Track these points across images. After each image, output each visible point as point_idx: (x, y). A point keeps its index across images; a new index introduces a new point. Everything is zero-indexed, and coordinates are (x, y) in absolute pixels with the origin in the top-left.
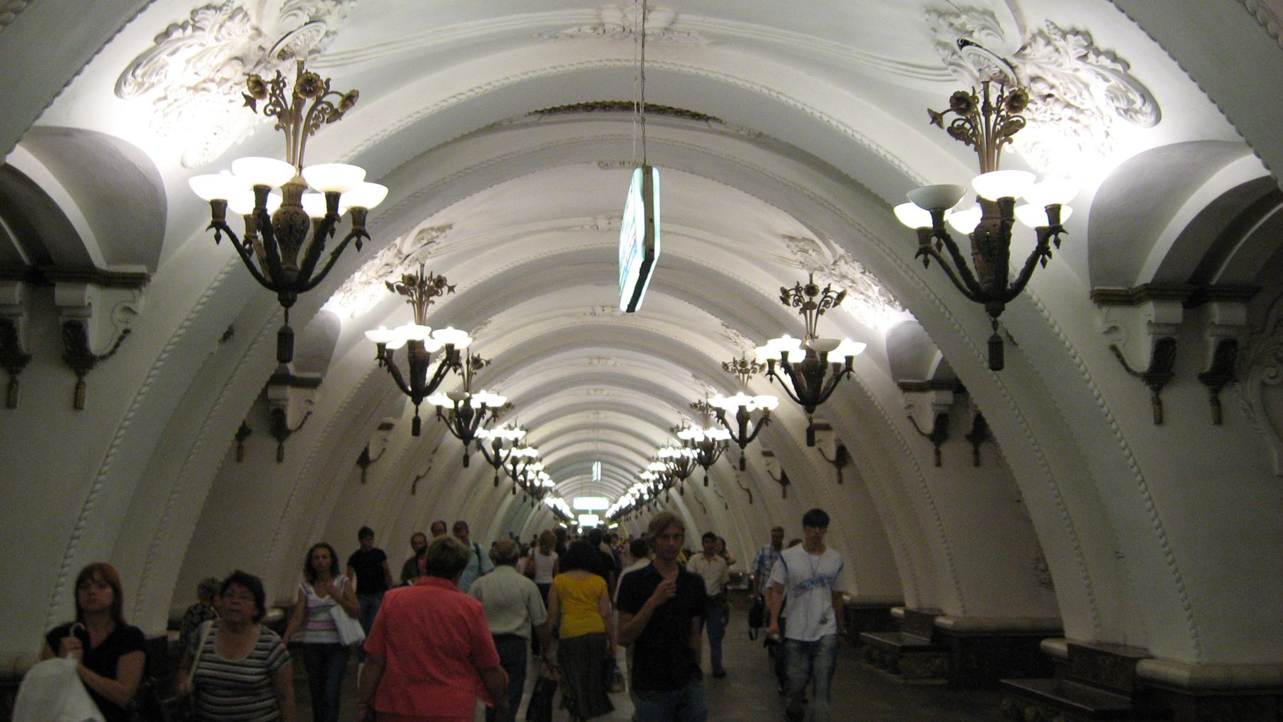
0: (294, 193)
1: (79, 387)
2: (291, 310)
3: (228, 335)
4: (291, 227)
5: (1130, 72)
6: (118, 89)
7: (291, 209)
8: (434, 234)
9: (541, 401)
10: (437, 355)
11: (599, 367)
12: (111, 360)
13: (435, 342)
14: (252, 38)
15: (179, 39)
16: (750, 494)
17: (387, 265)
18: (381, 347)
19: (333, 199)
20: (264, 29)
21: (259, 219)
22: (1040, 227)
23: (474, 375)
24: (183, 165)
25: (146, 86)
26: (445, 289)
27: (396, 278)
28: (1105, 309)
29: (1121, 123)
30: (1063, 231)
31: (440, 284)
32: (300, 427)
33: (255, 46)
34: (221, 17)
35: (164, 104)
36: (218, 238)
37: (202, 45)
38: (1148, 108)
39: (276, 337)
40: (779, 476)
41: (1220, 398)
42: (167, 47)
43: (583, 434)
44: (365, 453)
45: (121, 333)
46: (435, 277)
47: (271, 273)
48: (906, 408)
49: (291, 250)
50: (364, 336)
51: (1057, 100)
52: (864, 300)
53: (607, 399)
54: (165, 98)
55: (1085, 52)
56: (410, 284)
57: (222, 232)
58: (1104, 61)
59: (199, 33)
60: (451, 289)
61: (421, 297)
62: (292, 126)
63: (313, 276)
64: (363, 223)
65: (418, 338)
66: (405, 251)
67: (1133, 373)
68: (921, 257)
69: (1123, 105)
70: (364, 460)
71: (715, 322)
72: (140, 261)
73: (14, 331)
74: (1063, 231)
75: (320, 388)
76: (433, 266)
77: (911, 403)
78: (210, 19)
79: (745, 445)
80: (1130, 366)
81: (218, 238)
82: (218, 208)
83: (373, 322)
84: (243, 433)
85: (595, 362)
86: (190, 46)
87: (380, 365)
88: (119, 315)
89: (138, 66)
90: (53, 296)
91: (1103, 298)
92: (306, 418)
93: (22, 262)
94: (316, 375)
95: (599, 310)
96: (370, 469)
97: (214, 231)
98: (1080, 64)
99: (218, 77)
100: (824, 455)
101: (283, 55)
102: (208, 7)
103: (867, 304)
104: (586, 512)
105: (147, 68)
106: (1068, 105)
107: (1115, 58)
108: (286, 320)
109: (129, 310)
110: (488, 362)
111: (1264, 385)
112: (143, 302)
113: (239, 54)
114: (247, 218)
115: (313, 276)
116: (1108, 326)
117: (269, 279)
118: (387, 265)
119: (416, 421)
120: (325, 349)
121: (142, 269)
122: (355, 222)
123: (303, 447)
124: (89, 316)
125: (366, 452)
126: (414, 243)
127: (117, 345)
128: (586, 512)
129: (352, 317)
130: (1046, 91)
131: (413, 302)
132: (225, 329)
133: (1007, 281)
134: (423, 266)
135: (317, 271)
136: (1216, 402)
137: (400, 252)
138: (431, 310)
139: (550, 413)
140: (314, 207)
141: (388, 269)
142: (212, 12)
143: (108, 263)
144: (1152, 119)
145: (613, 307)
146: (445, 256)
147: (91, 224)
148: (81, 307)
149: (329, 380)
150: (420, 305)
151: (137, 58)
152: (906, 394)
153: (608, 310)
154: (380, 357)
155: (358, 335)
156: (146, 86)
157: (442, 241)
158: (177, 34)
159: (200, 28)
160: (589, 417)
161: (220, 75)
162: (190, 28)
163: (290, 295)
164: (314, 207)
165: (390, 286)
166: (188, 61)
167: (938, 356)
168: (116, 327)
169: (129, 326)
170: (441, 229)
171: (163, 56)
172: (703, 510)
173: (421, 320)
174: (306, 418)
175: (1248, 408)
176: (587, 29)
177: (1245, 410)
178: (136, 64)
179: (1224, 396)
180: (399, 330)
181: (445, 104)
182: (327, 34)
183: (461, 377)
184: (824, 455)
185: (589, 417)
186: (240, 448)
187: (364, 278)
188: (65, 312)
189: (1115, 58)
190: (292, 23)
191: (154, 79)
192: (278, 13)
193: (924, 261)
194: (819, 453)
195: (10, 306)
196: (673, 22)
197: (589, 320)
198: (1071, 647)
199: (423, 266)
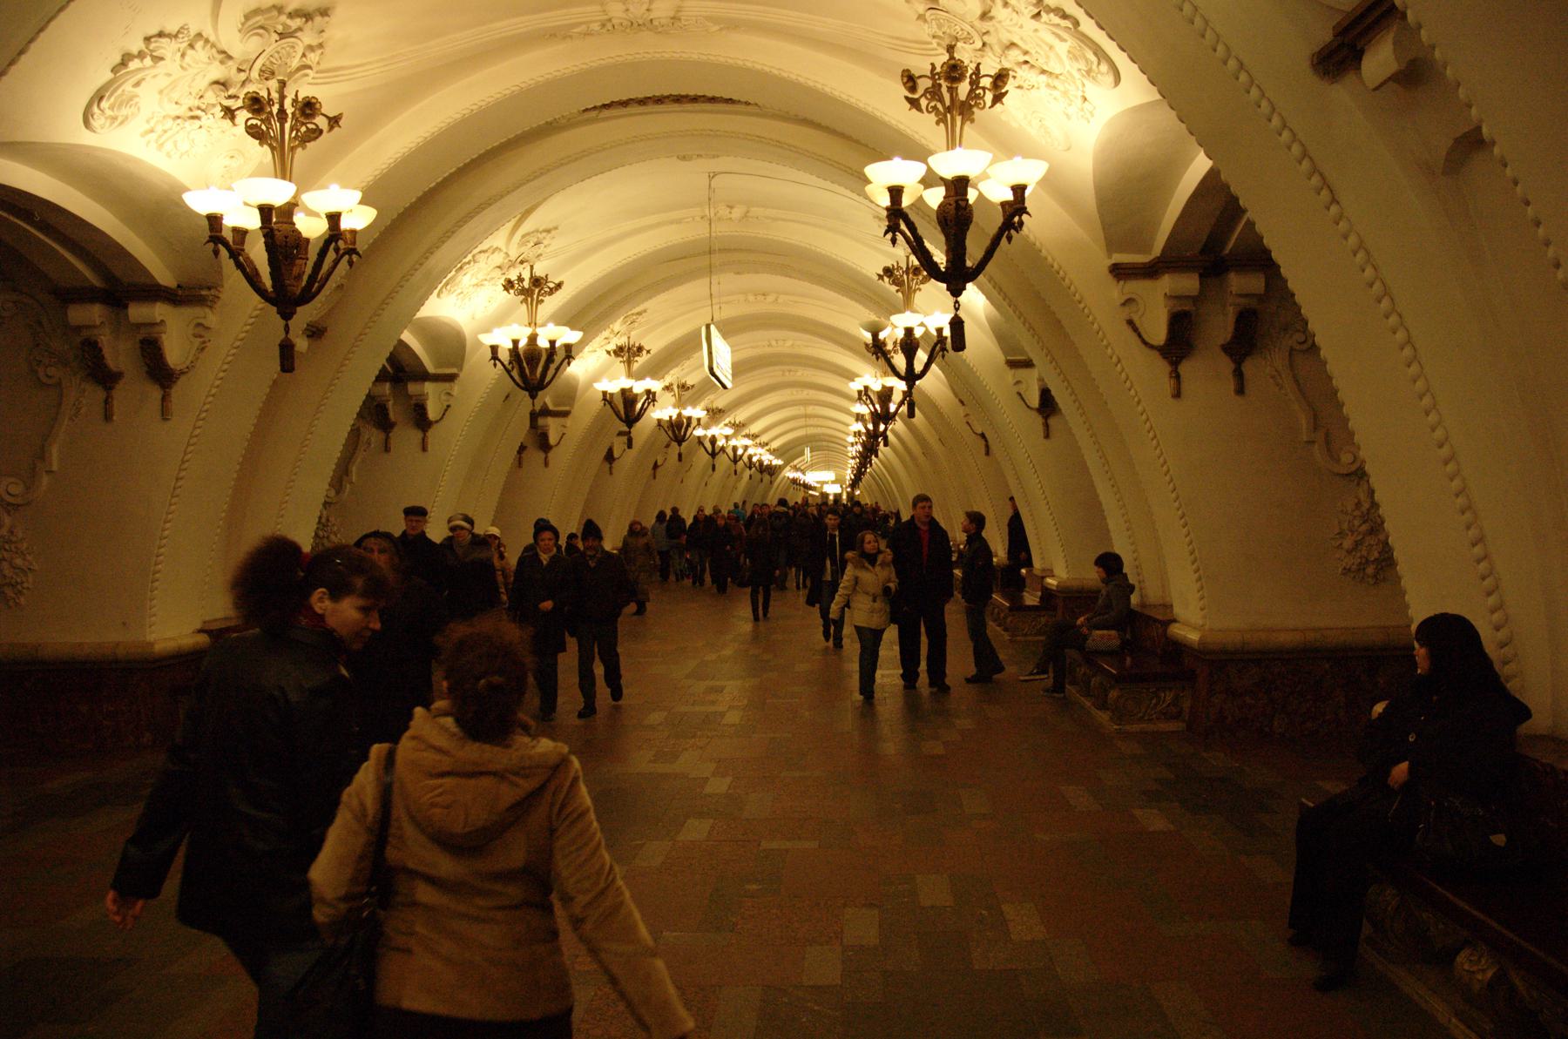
0: (533, 339)
1: (611, 468)
2: (535, 401)
3: (507, 397)
4: (532, 357)
5: (1080, 28)
6: (87, 123)
7: (532, 347)
8: (634, 317)
9: (754, 402)
10: (642, 395)
11: (789, 377)
12: (442, 422)
13: (639, 387)
14: (504, 259)
15: (139, 70)
16: (986, 441)
17: (606, 338)
18: (605, 393)
19: (334, 219)
20: (510, 253)
21: (514, 351)
22: (408, 508)
23: (918, 292)
24: (473, 318)
25: (120, 119)
26: (644, 352)
27: (612, 347)
28: (1013, 371)
29: (1091, 89)
30: (1028, 213)
31: (308, 112)
32: (559, 443)
33: (506, 261)
34: (487, 255)
35: (153, 136)
36: (495, 365)
37: (169, 75)
38: (1104, 67)
39: (528, 416)
40: (1035, 401)
41: (1243, 369)
42: (462, 272)
43: (802, 422)
44: (610, 451)
45: (445, 407)
46: (637, 345)
47: (524, 383)
48: (1124, 304)
49: (533, 369)
50: (592, 386)
51: (1033, 66)
52: (1048, 86)
53: (808, 397)
54: (462, 293)
55: (1036, 11)
56: (619, 351)
57: (497, 362)
58: (1056, 20)
59: (476, 264)
60: (648, 352)
61: (629, 357)
62: (529, 299)
63: (546, 381)
64: (571, 351)
65: (627, 386)
66: (616, 331)
67: (1152, 347)
68: (889, 236)
69: (1083, 66)
70: (656, 466)
71: (826, 342)
72: (453, 365)
73: (387, 410)
74: (1028, 213)
75: (570, 417)
76: (636, 338)
77: (1133, 296)
78: (167, 48)
79: (293, 313)
80: (1147, 339)
81: (495, 365)
82: (494, 349)
83: (596, 378)
84: (522, 448)
85: (787, 373)
86: (155, 76)
87: (605, 404)
88: (443, 397)
89: (101, 98)
90: (407, 389)
91: (1120, 272)
92: (562, 437)
93: (389, 372)
94: (567, 408)
95: (774, 343)
96: (615, 465)
97: (211, 245)
98: (1034, 24)
99: (488, 278)
100: (1140, 335)
101: (522, 262)
102: (161, 35)
103: (1055, 93)
104: (827, 483)
105: (112, 99)
106: (1043, 72)
107: (1065, 16)
108: (546, 458)
109: (449, 394)
110: (693, 386)
111: (1292, 349)
112: (456, 388)
113: (498, 265)
114: (510, 350)
115: (546, 381)
116: (1125, 298)
117: (522, 385)
118: (606, 338)
119: (680, 455)
120: (570, 393)
121: (454, 371)
122: (566, 351)
123: (562, 457)
124: (427, 399)
125: (610, 451)
126: (621, 325)
127: (444, 414)
128: (827, 483)
129: (473, 318)
130: (1022, 58)
131: (624, 362)
132: (506, 394)
133: (902, 352)
134: (629, 338)
135: (548, 379)
136: (1176, 376)
137: (613, 330)
138: (635, 366)
139: (757, 413)
140: (543, 343)
141: (607, 341)
142: (164, 41)
143: (436, 367)
144: (1110, 79)
145: (764, 295)
146: (644, 328)
147: (422, 344)
148: (153, 324)
149: (576, 411)
150: (629, 363)
151: (98, 90)
152: (1122, 283)
153: (780, 343)
154: (605, 399)
155: (589, 384)
156: (120, 119)
157: (641, 319)
158: (134, 65)
159: (162, 59)
160: (799, 410)
161: (489, 276)
162: (472, 263)
163: (535, 393)
164: (543, 343)
165: (608, 352)
166: (473, 275)
167: (1201, 164)
168: (442, 404)
169: (448, 403)
170: (639, 314)
171: (460, 277)
172: (983, 451)
173: (630, 375)
174: (562, 437)
175: (1276, 373)
176: (596, 27)
177: (1273, 377)
178: (99, 97)
179: (1248, 367)
180: (615, 382)
181: (619, 264)
182: (545, 247)
183: (674, 398)
184: (1140, 335)
185: (799, 410)
186: (520, 458)
187: (591, 349)
188: (414, 398)
189: (1065, 16)
190: (523, 249)
191: (124, 111)
192: (516, 246)
193: (213, 251)
194: (1016, 396)
195: (383, 396)
196: (748, 212)
197: (768, 350)
198: (893, 620)
199: (629, 338)
